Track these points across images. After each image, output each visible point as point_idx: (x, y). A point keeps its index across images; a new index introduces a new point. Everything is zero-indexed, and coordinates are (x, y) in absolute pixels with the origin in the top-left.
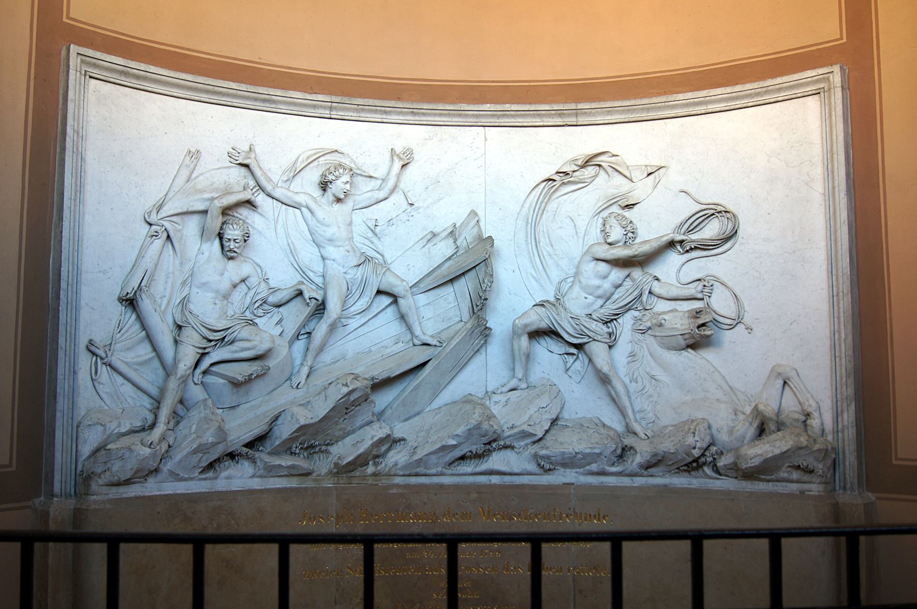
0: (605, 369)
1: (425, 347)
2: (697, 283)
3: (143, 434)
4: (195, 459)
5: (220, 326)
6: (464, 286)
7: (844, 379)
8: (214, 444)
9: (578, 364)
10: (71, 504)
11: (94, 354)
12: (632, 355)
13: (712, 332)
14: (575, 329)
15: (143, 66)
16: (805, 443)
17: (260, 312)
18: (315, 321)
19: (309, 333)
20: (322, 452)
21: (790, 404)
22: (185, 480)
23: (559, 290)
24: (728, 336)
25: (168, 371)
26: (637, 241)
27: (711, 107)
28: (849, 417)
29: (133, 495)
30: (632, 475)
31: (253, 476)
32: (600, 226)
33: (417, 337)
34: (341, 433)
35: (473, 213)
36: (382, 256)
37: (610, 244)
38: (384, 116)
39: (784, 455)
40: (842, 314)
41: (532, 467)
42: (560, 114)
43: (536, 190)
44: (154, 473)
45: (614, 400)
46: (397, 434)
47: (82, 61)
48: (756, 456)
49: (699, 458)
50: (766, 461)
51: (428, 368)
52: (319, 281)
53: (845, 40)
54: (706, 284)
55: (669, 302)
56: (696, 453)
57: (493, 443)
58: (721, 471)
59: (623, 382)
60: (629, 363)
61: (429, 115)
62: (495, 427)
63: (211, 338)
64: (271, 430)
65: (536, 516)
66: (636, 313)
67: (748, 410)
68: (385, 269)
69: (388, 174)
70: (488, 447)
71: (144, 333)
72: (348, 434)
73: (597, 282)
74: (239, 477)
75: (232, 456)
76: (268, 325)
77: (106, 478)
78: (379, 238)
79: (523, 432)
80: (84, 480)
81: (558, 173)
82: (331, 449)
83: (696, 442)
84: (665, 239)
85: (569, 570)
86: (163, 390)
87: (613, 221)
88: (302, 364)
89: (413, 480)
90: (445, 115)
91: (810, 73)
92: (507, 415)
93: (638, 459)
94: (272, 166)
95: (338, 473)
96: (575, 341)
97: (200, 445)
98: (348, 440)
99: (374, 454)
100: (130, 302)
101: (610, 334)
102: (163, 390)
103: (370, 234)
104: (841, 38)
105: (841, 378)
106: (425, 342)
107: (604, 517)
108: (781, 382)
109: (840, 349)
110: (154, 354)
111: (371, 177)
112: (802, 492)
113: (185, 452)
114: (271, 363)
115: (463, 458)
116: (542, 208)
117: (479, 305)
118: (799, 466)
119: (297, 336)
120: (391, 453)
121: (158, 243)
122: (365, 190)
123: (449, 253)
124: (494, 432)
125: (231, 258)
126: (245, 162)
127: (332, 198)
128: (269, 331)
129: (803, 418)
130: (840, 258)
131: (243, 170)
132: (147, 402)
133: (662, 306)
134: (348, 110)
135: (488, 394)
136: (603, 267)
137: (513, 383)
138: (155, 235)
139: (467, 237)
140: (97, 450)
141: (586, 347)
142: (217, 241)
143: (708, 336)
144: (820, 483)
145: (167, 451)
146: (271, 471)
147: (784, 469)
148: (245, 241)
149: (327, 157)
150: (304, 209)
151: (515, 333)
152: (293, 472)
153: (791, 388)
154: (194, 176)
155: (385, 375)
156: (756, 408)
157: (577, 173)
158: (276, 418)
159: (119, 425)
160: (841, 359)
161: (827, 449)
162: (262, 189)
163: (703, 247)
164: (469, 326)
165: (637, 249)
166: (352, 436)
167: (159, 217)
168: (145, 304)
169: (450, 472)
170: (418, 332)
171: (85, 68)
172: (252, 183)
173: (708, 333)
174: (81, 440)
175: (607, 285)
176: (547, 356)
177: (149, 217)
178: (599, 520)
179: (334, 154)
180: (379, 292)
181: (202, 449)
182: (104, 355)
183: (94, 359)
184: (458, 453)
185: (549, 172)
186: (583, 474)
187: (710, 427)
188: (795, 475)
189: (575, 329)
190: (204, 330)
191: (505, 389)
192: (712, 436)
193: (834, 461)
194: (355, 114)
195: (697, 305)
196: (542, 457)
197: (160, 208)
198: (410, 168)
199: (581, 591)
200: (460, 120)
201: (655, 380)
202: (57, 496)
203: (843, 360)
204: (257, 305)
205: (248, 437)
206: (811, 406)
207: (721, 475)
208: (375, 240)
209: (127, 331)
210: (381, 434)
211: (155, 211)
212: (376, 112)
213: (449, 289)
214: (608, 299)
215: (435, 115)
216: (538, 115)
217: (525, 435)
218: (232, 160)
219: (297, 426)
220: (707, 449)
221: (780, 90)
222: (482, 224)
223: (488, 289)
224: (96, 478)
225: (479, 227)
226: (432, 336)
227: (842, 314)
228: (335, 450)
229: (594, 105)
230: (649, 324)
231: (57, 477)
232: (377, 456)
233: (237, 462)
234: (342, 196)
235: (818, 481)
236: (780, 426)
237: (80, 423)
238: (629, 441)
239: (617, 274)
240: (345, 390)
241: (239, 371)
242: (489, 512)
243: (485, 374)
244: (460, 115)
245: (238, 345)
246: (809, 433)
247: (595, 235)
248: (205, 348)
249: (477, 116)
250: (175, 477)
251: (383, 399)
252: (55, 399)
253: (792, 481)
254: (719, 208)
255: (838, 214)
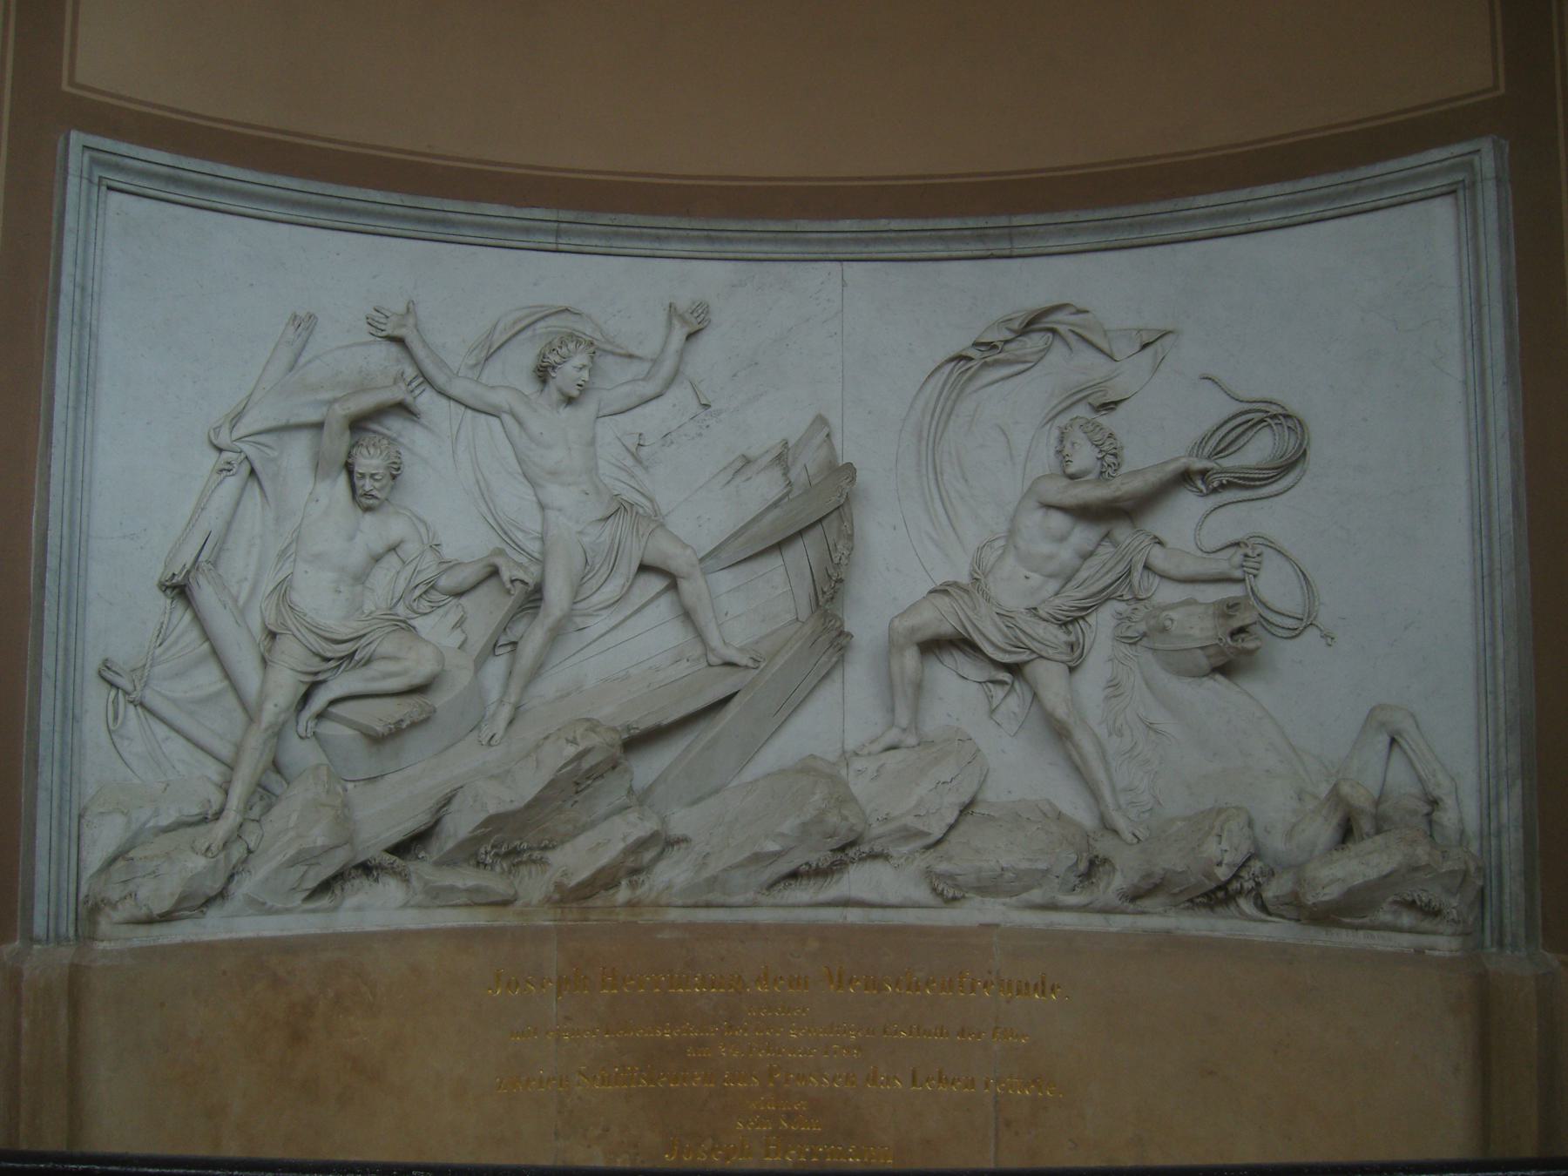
0: (1061, 712)
1: (728, 669)
2: (1231, 551)
3: (202, 829)
4: (294, 874)
5: (344, 632)
6: (800, 556)
7: (1502, 736)
8: (328, 850)
9: (1013, 703)
10: (66, 954)
11: (112, 685)
12: (1114, 685)
13: (1258, 643)
14: (1006, 636)
15: (208, 167)
16: (1424, 859)
17: (424, 605)
18: (525, 621)
19: (514, 644)
20: (534, 862)
21: (1400, 778)
22: (277, 912)
23: (978, 562)
24: (1286, 653)
25: (251, 715)
26: (1124, 469)
27: (1257, 220)
28: (1510, 809)
29: (178, 939)
30: (1106, 910)
31: (405, 906)
32: (1054, 442)
33: (713, 650)
34: (570, 827)
35: (821, 420)
36: (651, 501)
37: (1072, 477)
38: (656, 245)
39: (1386, 881)
40: (1498, 612)
41: (922, 893)
42: (980, 235)
43: (937, 376)
44: (219, 901)
45: (1080, 772)
46: (677, 829)
47: (93, 161)
48: (1332, 882)
49: (1229, 881)
50: (1350, 892)
51: (733, 708)
52: (534, 547)
53: (1502, 91)
54: (1250, 550)
55: (1182, 587)
56: (1223, 873)
57: (848, 850)
58: (1271, 908)
59: (1095, 735)
60: (1107, 698)
61: (740, 241)
62: (853, 820)
63: (329, 655)
64: (437, 822)
65: (927, 984)
66: (1121, 607)
67: (1324, 790)
68: (653, 526)
69: (663, 351)
70: (839, 856)
71: (206, 646)
72: (585, 828)
73: (1045, 548)
74: (378, 907)
75: (366, 869)
76: (436, 628)
77: (126, 910)
78: (646, 468)
79: (905, 828)
80: (90, 911)
81: (976, 344)
82: (550, 855)
83: (1222, 853)
84: (1171, 467)
85: (987, 1085)
86: (239, 748)
87: (1078, 436)
88: (501, 701)
89: (703, 916)
90: (769, 241)
91: (1435, 154)
92: (886, 795)
93: (1118, 882)
94: (449, 338)
95: (562, 901)
96: (1007, 659)
97: (299, 853)
98: (584, 841)
99: (631, 866)
100: (180, 590)
101: (1072, 646)
102: (239, 748)
103: (629, 462)
104: (1496, 87)
105: (1496, 735)
106: (728, 659)
107: (1053, 990)
108: (1385, 739)
109: (1495, 678)
110: (225, 683)
111: (631, 356)
112: (1419, 951)
113: (274, 864)
114: (439, 699)
115: (794, 875)
116: (947, 410)
117: (829, 592)
118: (1414, 902)
119: (493, 648)
120: (661, 866)
121: (232, 484)
122: (618, 382)
123: (775, 492)
124: (851, 830)
125: (368, 509)
126: (398, 333)
127: (555, 396)
128: (441, 637)
129: (1426, 809)
130: (1495, 504)
131: (394, 349)
132: (213, 771)
133: (1168, 593)
134: (588, 234)
135: (846, 757)
136: (1058, 521)
137: (892, 736)
138: (226, 469)
139: (809, 462)
140: (113, 860)
141: (1028, 670)
142: (342, 480)
143: (1250, 652)
144: (1453, 935)
145: (245, 861)
146: (438, 896)
147: (1385, 906)
148: (394, 477)
149: (552, 321)
150: (506, 417)
151: (893, 646)
152: (477, 899)
153: (1405, 753)
154: (303, 360)
155: (649, 722)
156: (1335, 790)
157: (1012, 346)
158: (448, 800)
159: (156, 813)
160: (1496, 698)
161: (1466, 873)
162: (427, 381)
163: (1244, 482)
164: (807, 630)
165: (1123, 486)
166: (589, 833)
167: (236, 435)
168: (205, 593)
169: (771, 900)
170: (714, 640)
171: (98, 172)
172: (410, 372)
173: (1250, 645)
174: (86, 840)
175: (1066, 554)
176: (955, 690)
177: (217, 435)
178: (1043, 993)
179: (564, 316)
180: (644, 568)
181: (304, 858)
182: (129, 687)
183: (113, 693)
184: (785, 867)
185: (960, 342)
186: (1017, 908)
187: (1250, 824)
188: (1406, 919)
189: (1006, 636)
190: (312, 638)
191: (878, 747)
192: (1255, 842)
193: (1482, 890)
194: (603, 243)
195: (1234, 591)
196: (940, 876)
197: (237, 418)
198: (704, 340)
199: (1008, 1124)
200: (796, 249)
201: (1156, 732)
202: (39, 942)
203: (1501, 700)
204: (418, 592)
205: (396, 834)
206: (1443, 789)
207: (1270, 914)
208: (638, 472)
209: (176, 642)
210: (649, 826)
211: (227, 425)
212: (640, 237)
213: (774, 562)
214: (1069, 580)
215: (750, 241)
216: (941, 238)
217: (908, 834)
218: (373, 330)
219: (482, 816)
220: (1243, 865)
221: (1382, 186)
222: (837, 441)
223: (844, 561)
224: (107, 909)
225: (832, 447)
226: (741, 650)
227: (1498, 612)
228: (558, 858)
229: (1042, 219)
230: (1142, 627)
231: (40, 907)
232: (636, 871)
233: (377, 880)
234: (575, 392)
235: (1449, 930)
236: (1381, 824)
237: (85, 809)
238: (1104, 846)
239: (1084, 536)
240: (571, 751)
241: (380, 715)
242: (840, 976)
243: (840, 719)
244: (795, 242)
245: (378, 667)
246: (1438, 839)
247: (1045, 459)
248: (316, 674)
249: (829, 242)
250: (259, 907)
251: (648, 767)
252: (36, 767)
253: (1401, 930)
254: (1274, 410)
255: (1491, 419)
